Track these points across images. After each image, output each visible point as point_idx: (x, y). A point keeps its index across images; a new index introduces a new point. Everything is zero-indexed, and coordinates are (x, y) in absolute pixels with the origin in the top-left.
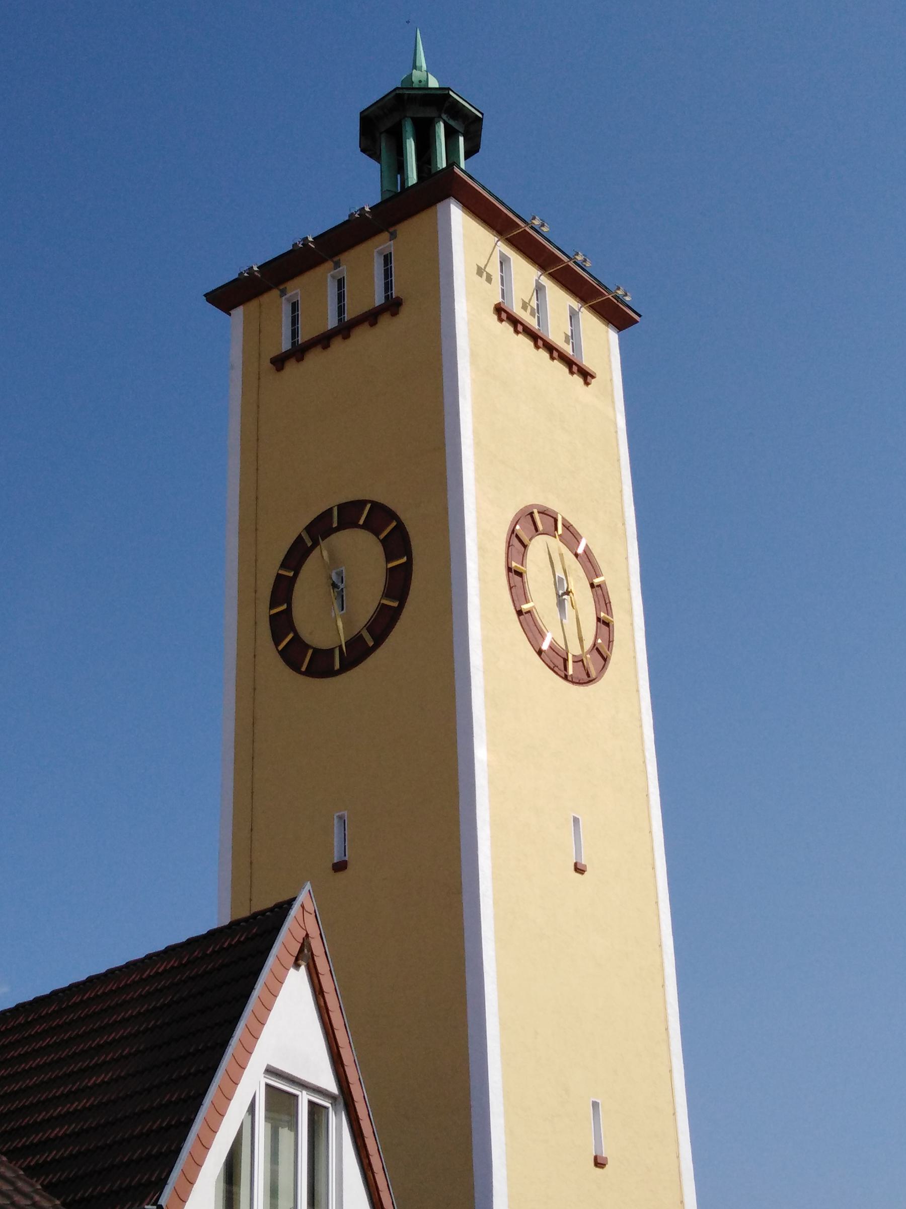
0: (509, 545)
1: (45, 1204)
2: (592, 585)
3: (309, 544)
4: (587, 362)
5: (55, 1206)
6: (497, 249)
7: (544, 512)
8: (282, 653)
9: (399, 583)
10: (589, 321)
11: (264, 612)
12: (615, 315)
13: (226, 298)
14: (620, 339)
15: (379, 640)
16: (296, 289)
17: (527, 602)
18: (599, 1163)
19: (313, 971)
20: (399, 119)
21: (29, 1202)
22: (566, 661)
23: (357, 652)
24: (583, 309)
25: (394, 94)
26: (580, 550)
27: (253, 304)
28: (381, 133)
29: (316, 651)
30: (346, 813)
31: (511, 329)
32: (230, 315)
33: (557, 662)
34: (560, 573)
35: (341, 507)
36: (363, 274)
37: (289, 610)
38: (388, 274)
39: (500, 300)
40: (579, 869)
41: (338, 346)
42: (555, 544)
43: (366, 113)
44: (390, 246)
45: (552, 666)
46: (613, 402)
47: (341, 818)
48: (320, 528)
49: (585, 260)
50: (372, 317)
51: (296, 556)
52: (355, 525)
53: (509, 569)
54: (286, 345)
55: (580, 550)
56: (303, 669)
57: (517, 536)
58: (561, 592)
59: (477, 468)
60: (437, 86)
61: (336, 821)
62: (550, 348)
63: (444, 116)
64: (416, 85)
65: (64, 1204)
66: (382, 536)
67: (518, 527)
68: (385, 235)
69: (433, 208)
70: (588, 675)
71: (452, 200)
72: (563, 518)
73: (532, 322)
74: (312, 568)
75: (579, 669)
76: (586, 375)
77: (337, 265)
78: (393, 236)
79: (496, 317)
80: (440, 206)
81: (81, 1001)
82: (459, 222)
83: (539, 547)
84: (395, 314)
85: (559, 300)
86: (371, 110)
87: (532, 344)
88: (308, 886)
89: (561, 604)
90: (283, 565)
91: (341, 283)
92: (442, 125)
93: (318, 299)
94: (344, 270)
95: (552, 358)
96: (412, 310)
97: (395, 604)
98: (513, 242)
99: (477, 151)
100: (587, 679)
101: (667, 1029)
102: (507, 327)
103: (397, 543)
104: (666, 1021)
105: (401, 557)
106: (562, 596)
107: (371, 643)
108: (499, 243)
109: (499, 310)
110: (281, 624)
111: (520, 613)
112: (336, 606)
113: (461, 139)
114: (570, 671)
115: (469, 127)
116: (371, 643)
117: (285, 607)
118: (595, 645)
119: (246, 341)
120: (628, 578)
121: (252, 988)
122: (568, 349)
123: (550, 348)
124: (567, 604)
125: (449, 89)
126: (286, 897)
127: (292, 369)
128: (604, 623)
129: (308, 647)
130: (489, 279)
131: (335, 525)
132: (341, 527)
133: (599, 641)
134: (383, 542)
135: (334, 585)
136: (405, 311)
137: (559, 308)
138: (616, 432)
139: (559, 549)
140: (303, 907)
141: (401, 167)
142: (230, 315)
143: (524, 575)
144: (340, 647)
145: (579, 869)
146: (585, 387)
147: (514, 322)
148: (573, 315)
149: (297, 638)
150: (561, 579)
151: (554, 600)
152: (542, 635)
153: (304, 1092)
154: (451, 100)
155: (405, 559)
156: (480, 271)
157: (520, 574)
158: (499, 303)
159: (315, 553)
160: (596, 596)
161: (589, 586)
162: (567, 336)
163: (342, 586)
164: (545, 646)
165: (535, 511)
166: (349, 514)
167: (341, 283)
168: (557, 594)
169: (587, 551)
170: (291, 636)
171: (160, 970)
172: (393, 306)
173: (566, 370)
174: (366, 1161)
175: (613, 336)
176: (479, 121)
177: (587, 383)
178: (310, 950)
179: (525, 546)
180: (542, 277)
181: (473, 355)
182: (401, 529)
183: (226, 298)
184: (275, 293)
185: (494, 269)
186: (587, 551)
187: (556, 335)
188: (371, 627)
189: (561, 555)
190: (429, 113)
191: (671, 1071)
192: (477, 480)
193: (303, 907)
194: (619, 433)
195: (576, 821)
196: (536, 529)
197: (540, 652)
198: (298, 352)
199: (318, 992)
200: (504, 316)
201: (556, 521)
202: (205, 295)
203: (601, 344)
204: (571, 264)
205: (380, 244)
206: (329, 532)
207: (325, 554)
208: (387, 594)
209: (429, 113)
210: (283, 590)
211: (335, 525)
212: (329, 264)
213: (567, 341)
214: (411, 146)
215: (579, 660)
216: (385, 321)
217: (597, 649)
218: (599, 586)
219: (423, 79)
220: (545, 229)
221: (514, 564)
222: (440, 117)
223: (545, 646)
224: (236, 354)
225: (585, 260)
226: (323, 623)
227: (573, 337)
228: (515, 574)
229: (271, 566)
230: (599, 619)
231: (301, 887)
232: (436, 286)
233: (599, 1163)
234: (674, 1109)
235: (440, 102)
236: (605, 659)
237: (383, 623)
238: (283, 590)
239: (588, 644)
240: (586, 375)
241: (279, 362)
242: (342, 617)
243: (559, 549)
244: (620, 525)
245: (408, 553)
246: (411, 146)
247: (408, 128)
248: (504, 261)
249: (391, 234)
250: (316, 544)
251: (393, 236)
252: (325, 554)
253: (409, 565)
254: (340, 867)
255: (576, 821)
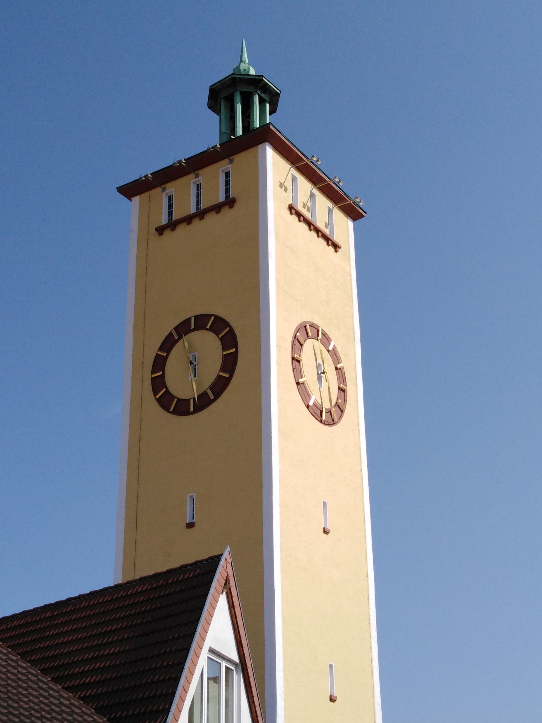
0: (293, 344)
1: (101, 721)
2: (336, 368)
3: (176, 338)
4: (336, 239)
5: (104, 721)
6: (291, 172)
7: (311, 326)
8: (158, 400)
9: (230, 363)
10: (339, 215)
11: (148, 375)
12: (353, 212)
13: (130, 190)
14: (354, 225)
15: (217, 396)
16: (172, 188)
17: (302, 378)
18: (332, 699)
19: (229, 595)
20: (233, 92)
21: (92, 719)
22: (321, 412)
23: (203, 402)
24: (335, 208)
25: (230, 77)
26: (331, 348)
27: (145, 196)
28: (221, 99)
29: (179, 400)
30: (195, 494)
31: (297, 219)
32: (131, 200)
33: (317, 412)
34: (320, 361)
35: (196, 317)
36: (212, 183)
37: (163, 376)
38: (227, 183)
39: (291, 202)
40: (326, 532)
41: (196, 223)
42: (318, 344)
43: (213, 87)
44: (229, 167)
45: (314, 414)
46: (350, 263)
47: (191, 497)
48: (183, 329)
49: (340, 181)
50: (217, 208)
51: (168, 344)
52: (205, 328)
53: (293, 358)
54: (164, 221)
55: (331, 348)
56: (171, 410)
57: (298, 340)
58: (320, 372)
59: (277, 300)
60: (254, 74)
61: (188, 499)
62: (317, 231)
63: (259, 92)
64: (242, 72)
65: (108, 720)
66: (220, 336)
67: (298, 334)
68: (227, 161)
69: (256, 147)
70: (333, 420)
71: (267, 143)
72: (322, 329)
73: (308, 215)
74: (177, 352)
75: (328, 416)
76: (336, 247)
77: (197, 176)
78: (231, 162)
79: (289, 212)
80: (260, 146)
81: (89, 605)
82: (270, 155)
83: (309, 345)
84: (231, 207)
85: (323, 203)
86: (216, 85)
87: (308, 228)
88: (228, 548)
89: (320, 379)
90: (160, 349)
91: (199, 187)
92: (257, 96)
93: (184, 195)
94: (201, 179)
95: (318, 236)
96: (240, 205)
97: (227, 376)
98: (299, 169)
99: (276, 112)
100: (332, 423)
101: (369, 624)
102: (295, 218)
103: (229, 340)
104: (369, 619)
105: (232, 349)
106: (321, 374)
107: (212, 397)
108: (292, 169)
109: (291, 208)
110: (158, 383)
111: (298, 384)
112: (192, 375)
113: (268, 105)
114: (324, 418)
115: (272, 98)
116: (212, 397)
117: (161, 373)
118: (337, 403)
119: (140, 218)
120: (355, 364)
121: (204, 605)
122: (326, 231)
123: (317, 231)
124: (323, 379)
125: (263, 76)
126: (216, 553)
127: (168, 233)
128: (342, 390)
129: (174, 397)
130: (286, 190)
131: (192, 327)
132: (197, 328)
133: (340, 401)
134: (220, 339)
135: (191, 363)
136: (237, 205)
137: (322, 208)
138: (351, 280)
139: (320, 347)
140: (226, 559)
141: (232, 119)
142: (131, 200)
143: (301, 362)
144: (194, 399)
145: (326, 532)
146: (335, 254)
147: (299, 215)
148: (330, 211)
149: (167, 392)
150: (320, 365)
151: (316, 377)
152: (309, 397)
153: (224, 662)
154: (263, 82)
155: (234, 350)
156: (281, 185)
157: (298, 361)
158: (291, 204)
159: (180, 343)
160: (338, 375)
161: (334, 369)
162: (326, 223)
163: (195, 363)
164: (311, 403)
165: (308, 325)
166: (201, 322)
167: (199, 187)
168: (318, 373)
169: (334, 348)
170: (164, 390)
171: (139, 590)
172: (230, 202)
173: (325, 243)
174: (251, 700)
175: (350, 224)
176: (278, 95)
177: (336, 251)
178: (229, 584)
179: (301, 345)
180: (314, 189)
181: (277, 234)
182: (232, 332)
183: (130, 190)
184: (159, 190)
185: (289, 184)
186: (334, 348)
187: (320, 224)
188: (212, 388)
189: (321, 351)
190: (250, 89)
191: (371, 648)
192: (277, 307)
193: (226, 559)
194: (352, 280)
195: (325, 503)
196: (308, 336)
197: (308, 407)
198: (172, 225)
199: (231, 607)
200: (293, 211)
201: (318, 331)
202: (117, 188)
203: (344, 228)
204: (331, 183)
205: (223, 166)
206: (188, 331)
207: (186, 344)
208: (222, 369)
209: (250, 89)
210: (159, 364)
211: (192, 327)
212: (192, 175)
213: (326, 227)
214: (239, 108)
215: (329, 412)
216: (225, 210)
217: (338, 405)
218: (340, 369)
219: (247, 69)
220: (321, 164)
221: (296, 356)
222: (257, 92)
223: (311, 403)
224: (134, 224)
225: (340, 181)
226: (184, 384)
227: (330, 224)
228: (296, 361)
229: (152, 350)
230: (339, 388)
231: (225, 549)
232: (257, 192)
233: (332, 699)
234: (372, 669)
235: (257, 83)
236: (342, 411)
237: (220, 386)
238: (159, 364)
239: (334, 403)
240: (336, 247)
241: (160, 230)
242: (196, 381)
243: (320, 347)
244: (352, 334)
245: (235, 345)
246: (239, 108)
247: (238, 98)
248: (294, 179)
249: (230, 160)
250: (180, 337)
251: (231, 162)
252: (186, 344)
253: (236, 354)
254: (190, 525)
255: (325, 503)
